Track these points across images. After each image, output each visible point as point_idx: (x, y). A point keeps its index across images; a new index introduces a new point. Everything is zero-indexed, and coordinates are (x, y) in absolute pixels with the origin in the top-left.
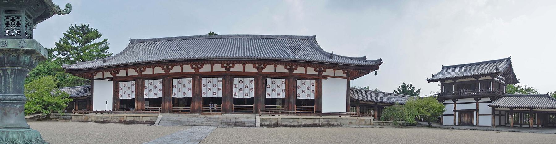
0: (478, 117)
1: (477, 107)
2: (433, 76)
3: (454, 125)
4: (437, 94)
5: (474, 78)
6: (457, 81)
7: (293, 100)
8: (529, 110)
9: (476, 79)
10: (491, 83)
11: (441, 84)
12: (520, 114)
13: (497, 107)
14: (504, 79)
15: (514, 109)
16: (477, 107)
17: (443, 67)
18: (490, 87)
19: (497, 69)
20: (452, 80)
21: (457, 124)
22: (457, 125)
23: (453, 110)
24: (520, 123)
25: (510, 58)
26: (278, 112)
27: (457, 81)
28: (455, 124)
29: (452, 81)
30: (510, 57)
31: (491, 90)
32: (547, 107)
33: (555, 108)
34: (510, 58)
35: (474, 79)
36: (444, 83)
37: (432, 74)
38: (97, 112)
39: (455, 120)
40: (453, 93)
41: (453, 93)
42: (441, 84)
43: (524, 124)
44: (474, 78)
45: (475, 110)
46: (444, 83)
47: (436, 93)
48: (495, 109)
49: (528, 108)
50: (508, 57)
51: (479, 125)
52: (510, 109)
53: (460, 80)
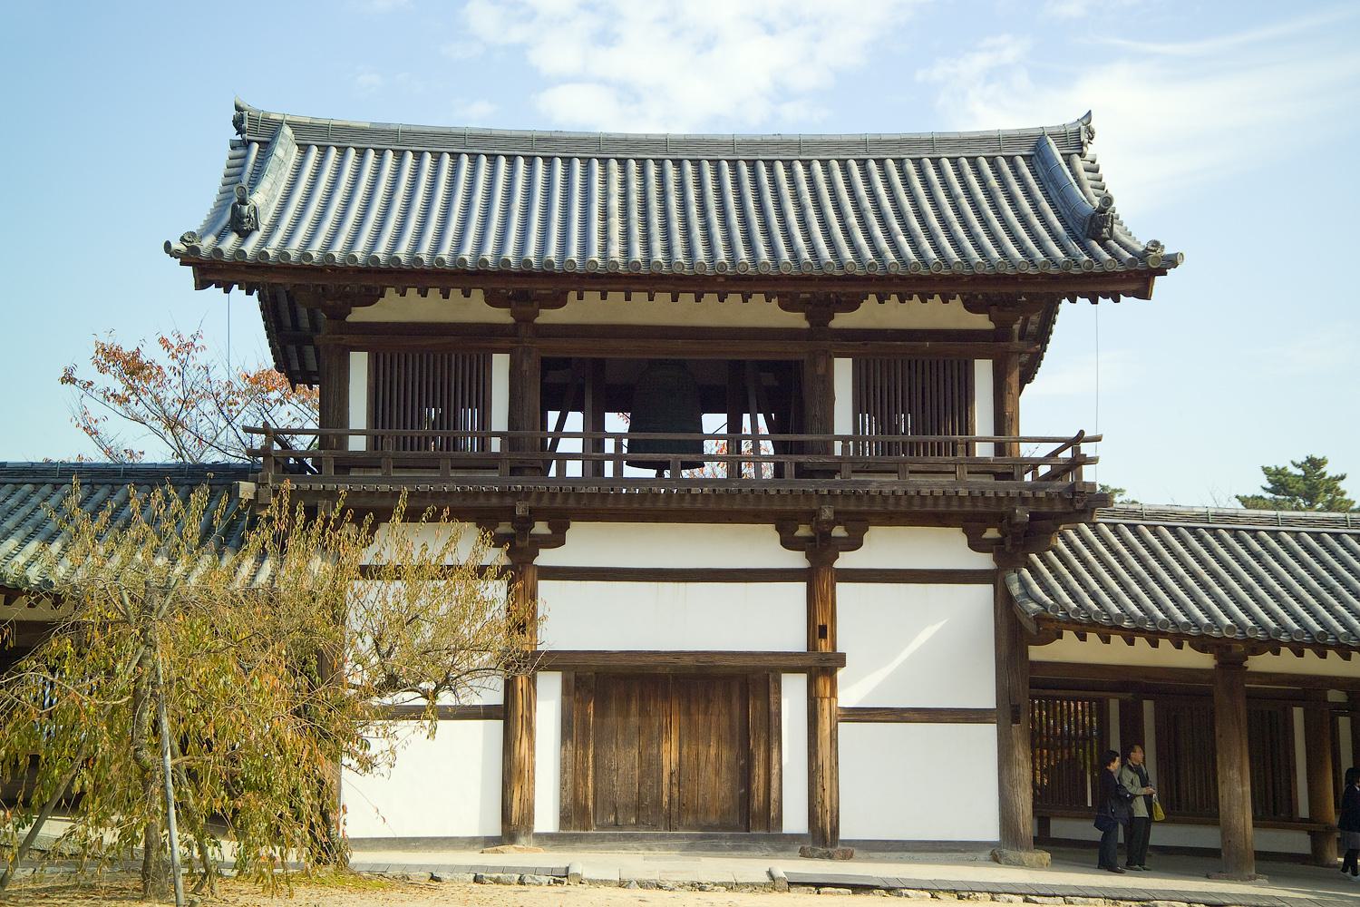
1: (820, 627)
6: (548, 316)
7: (347, 339)
12: (1114, 706)
15: (1261, 663)
16: (820, 627)
18: (484, 405)
20: (956, 305)
21: (546, 818)
22: (547, 839)
24: (1304, 811)
26: (522, 689)
27: (548, 316)
28: (513, 826)
29: (475, 309)
35: (763, 313)
39: (513, 773)
45: (785, 662)
51: (843, 835)
52: (1206, 661)
53: (581, 310)
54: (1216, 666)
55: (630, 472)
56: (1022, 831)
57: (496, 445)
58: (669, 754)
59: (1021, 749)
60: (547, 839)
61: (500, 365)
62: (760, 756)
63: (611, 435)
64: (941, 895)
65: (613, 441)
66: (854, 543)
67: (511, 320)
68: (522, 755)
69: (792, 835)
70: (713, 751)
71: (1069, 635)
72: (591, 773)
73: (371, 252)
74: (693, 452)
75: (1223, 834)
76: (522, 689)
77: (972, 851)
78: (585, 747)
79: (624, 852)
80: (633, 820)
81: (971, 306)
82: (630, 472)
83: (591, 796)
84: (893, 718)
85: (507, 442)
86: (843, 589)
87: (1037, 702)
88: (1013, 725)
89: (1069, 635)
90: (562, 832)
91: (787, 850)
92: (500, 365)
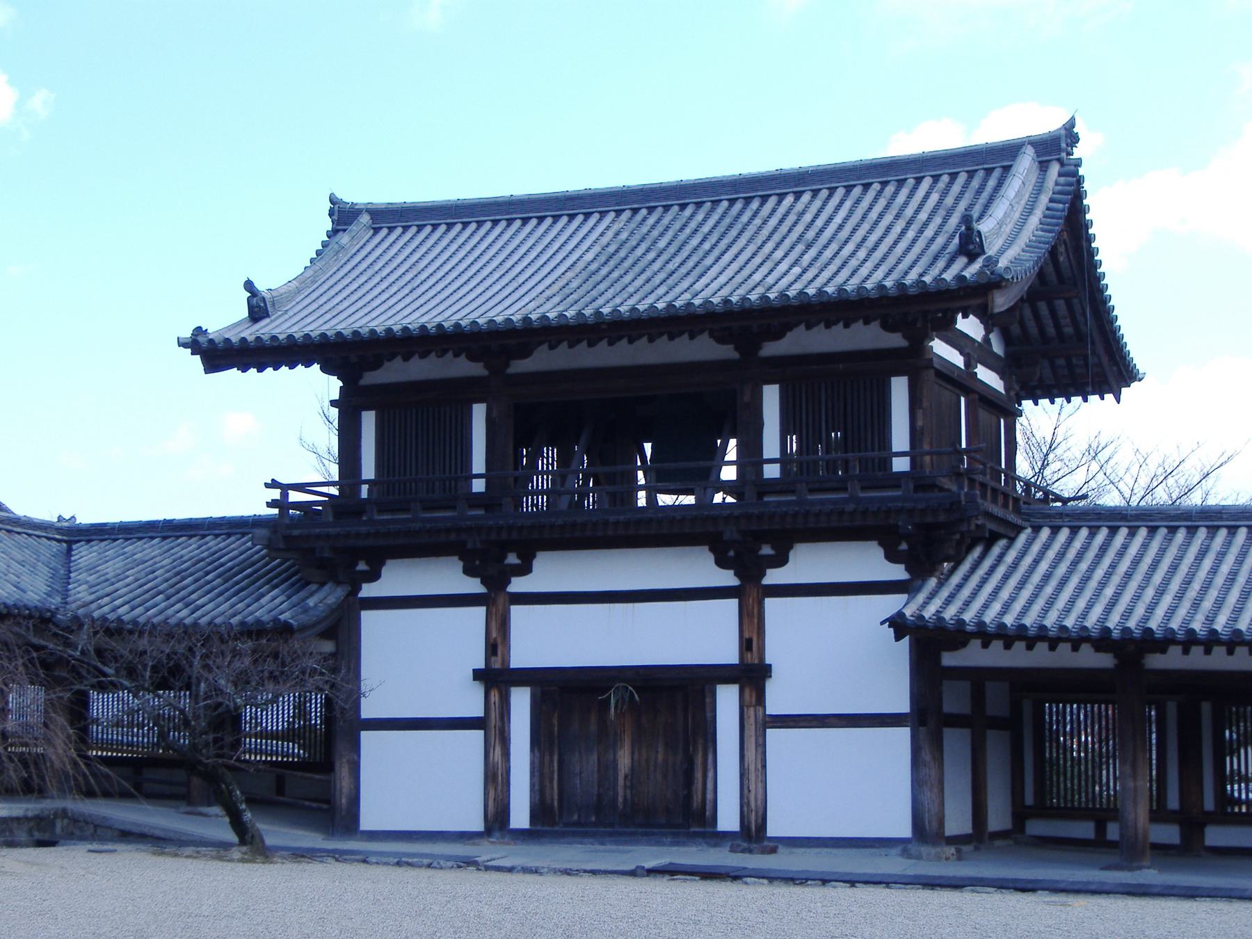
0: (762, 746)
2: (258, 309)
3: (488, 832)
4: (295, 496)
5: (463, 358)
8: (1105, 661)
9: (727, 352)
10: (899, 388)
11: (333, 386)
13: (957, 636)
14: (997, 348)
17: (343, 215)
19: (970, 245)
20: (875, 326)
21: (520, 817)
22: (521, 835)
23: (478, 675)
25: (1069, 136)
26: (495, 703)
27: (519, 366)
28: (497, 819)
29: (463, 367)
30: (1071, 124)
31: (901, 465)
32: (1181, 635)
33: (1235, 641)
34: (1069, 136)
35: (704, 349)
36: (371, 378)
37: (249, 285)
38: (374, 835)
40: (479, 486)
41: (479, 486)
42: (333, 386)
43: (1043, 810)
44: (463, 358)
46: (371, 378)
47: (285, 488)
48: (949, 659)
49: (1103, 641)
50: (1046, 123)
53: (542, 360)
54: (1116, 665)
55: (665, 500)
56: (927, 828)
57: (364, 491)
58: (624, 760)
59: (928, 752)
60: (521, 835)
61: (479, 413)
62: (699, 760)
63: (366, 482)
64: (857, 885)
65: (367, 486)
66: (780, 560)
67: (485, 373)
68: (496, 760)
69: (723, 832)
70: (660, 757)
71: (976, 644)
72: (556, 776)
73: (962, 271)
74: (705, 479)
75: (1121, 829)
76: (495, 703)
77: (884, 847)
78: (551, 755)
79: (580, 846)
80: (593, 819)
81: (887, 327)
82: (665, 500)
83: (556, 797)
84: (815, 723)
85: (653, 475)
86: (771, 604)
87: (1234, 709)
88: (921, 728)
89: (976, 644)
90: (533, 828)
91: (720, 846)
92: (479, 413)
